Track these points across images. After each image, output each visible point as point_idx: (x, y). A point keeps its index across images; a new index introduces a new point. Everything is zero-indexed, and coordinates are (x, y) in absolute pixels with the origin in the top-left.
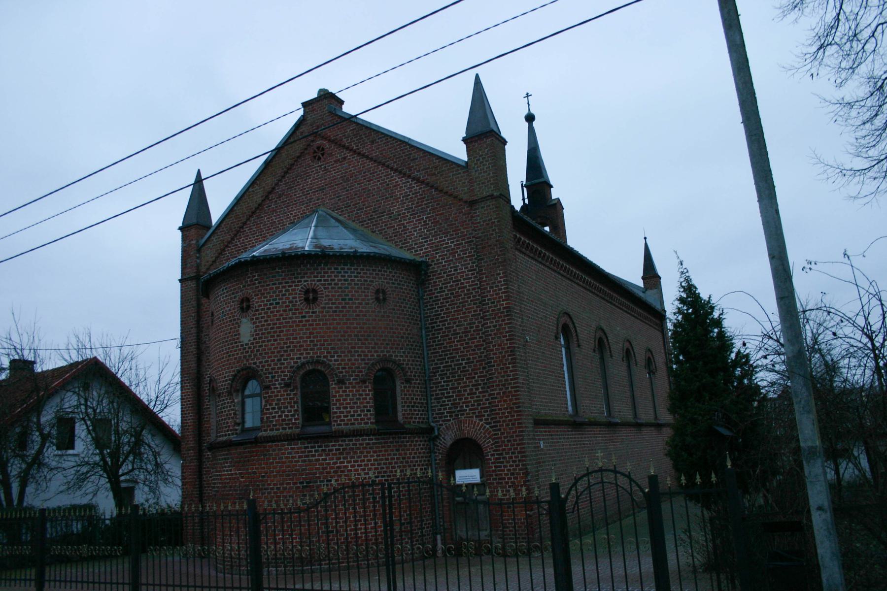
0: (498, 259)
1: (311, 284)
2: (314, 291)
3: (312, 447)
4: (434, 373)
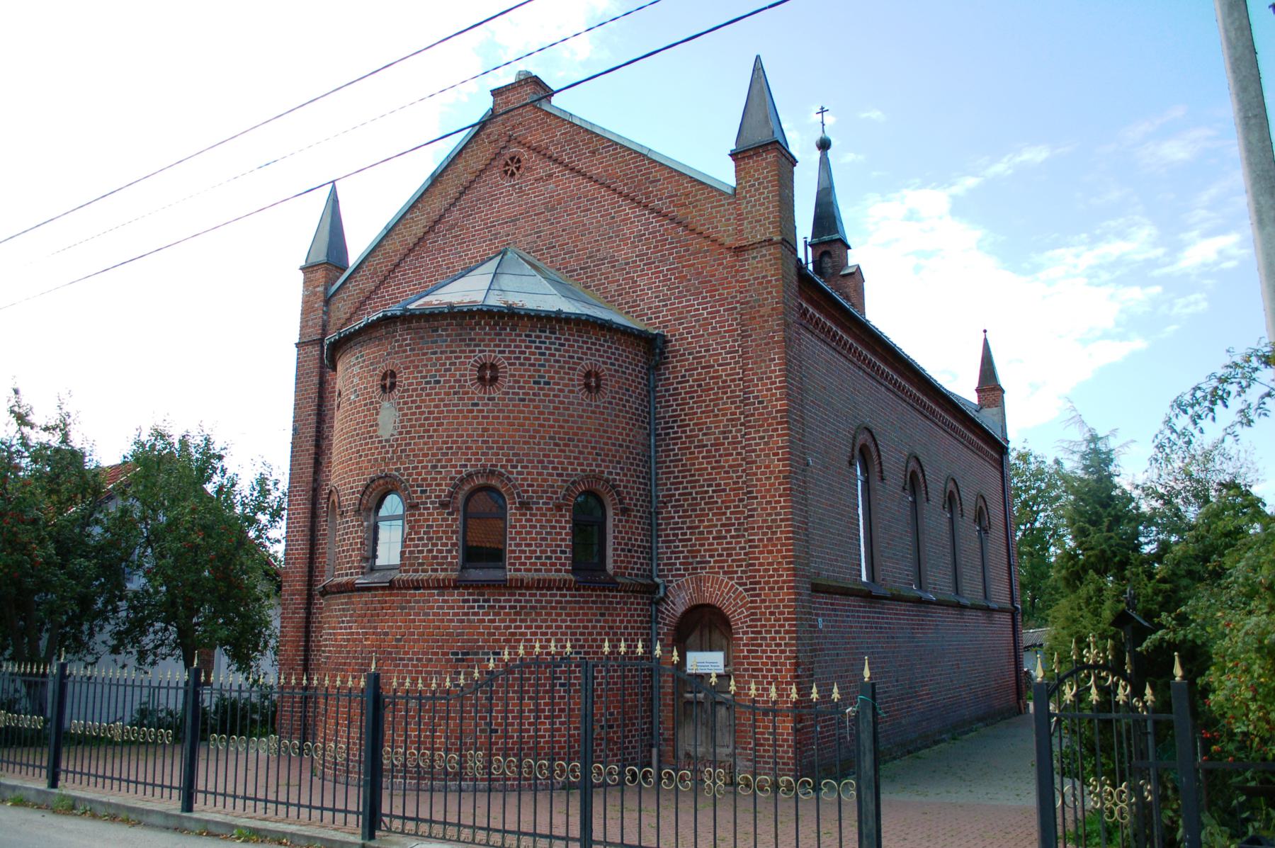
2: (493, 367)
3: (474, 601)
4: (665, 503)
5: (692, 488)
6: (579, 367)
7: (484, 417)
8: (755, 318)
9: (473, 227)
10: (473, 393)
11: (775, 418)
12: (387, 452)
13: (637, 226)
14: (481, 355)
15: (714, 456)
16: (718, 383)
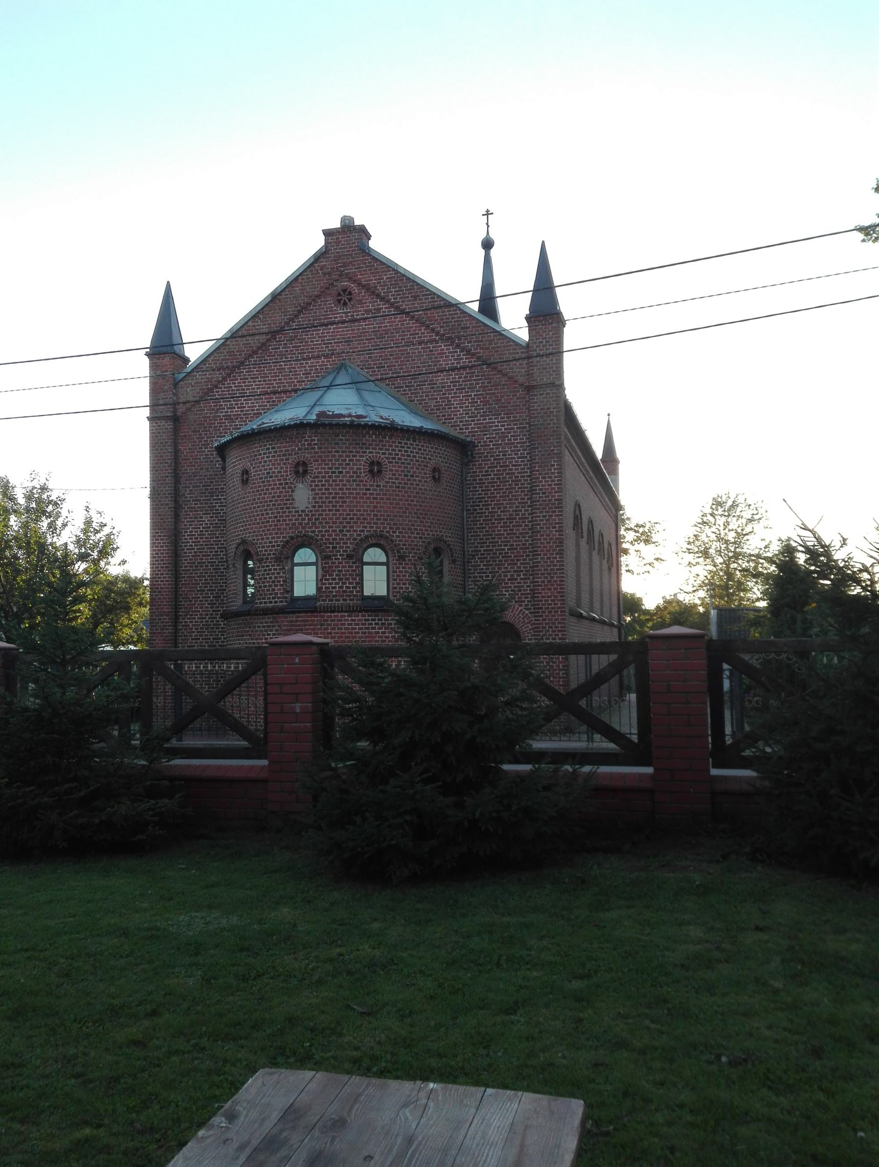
0: (553, 450)
1: (377, 456)
2: (379, 463)
3: (372, 620)
4: (473, 556)
5: (493, 546)
6: (429, 465)
7: (374, 498)
8: (541, 437)
9: (312, 341)
10: (366, 481)
11: (554, 504)
12: (304, 519)
13: (451, 360)
14: (371, 455)
15: (509, 526)
16: (512, 478)
